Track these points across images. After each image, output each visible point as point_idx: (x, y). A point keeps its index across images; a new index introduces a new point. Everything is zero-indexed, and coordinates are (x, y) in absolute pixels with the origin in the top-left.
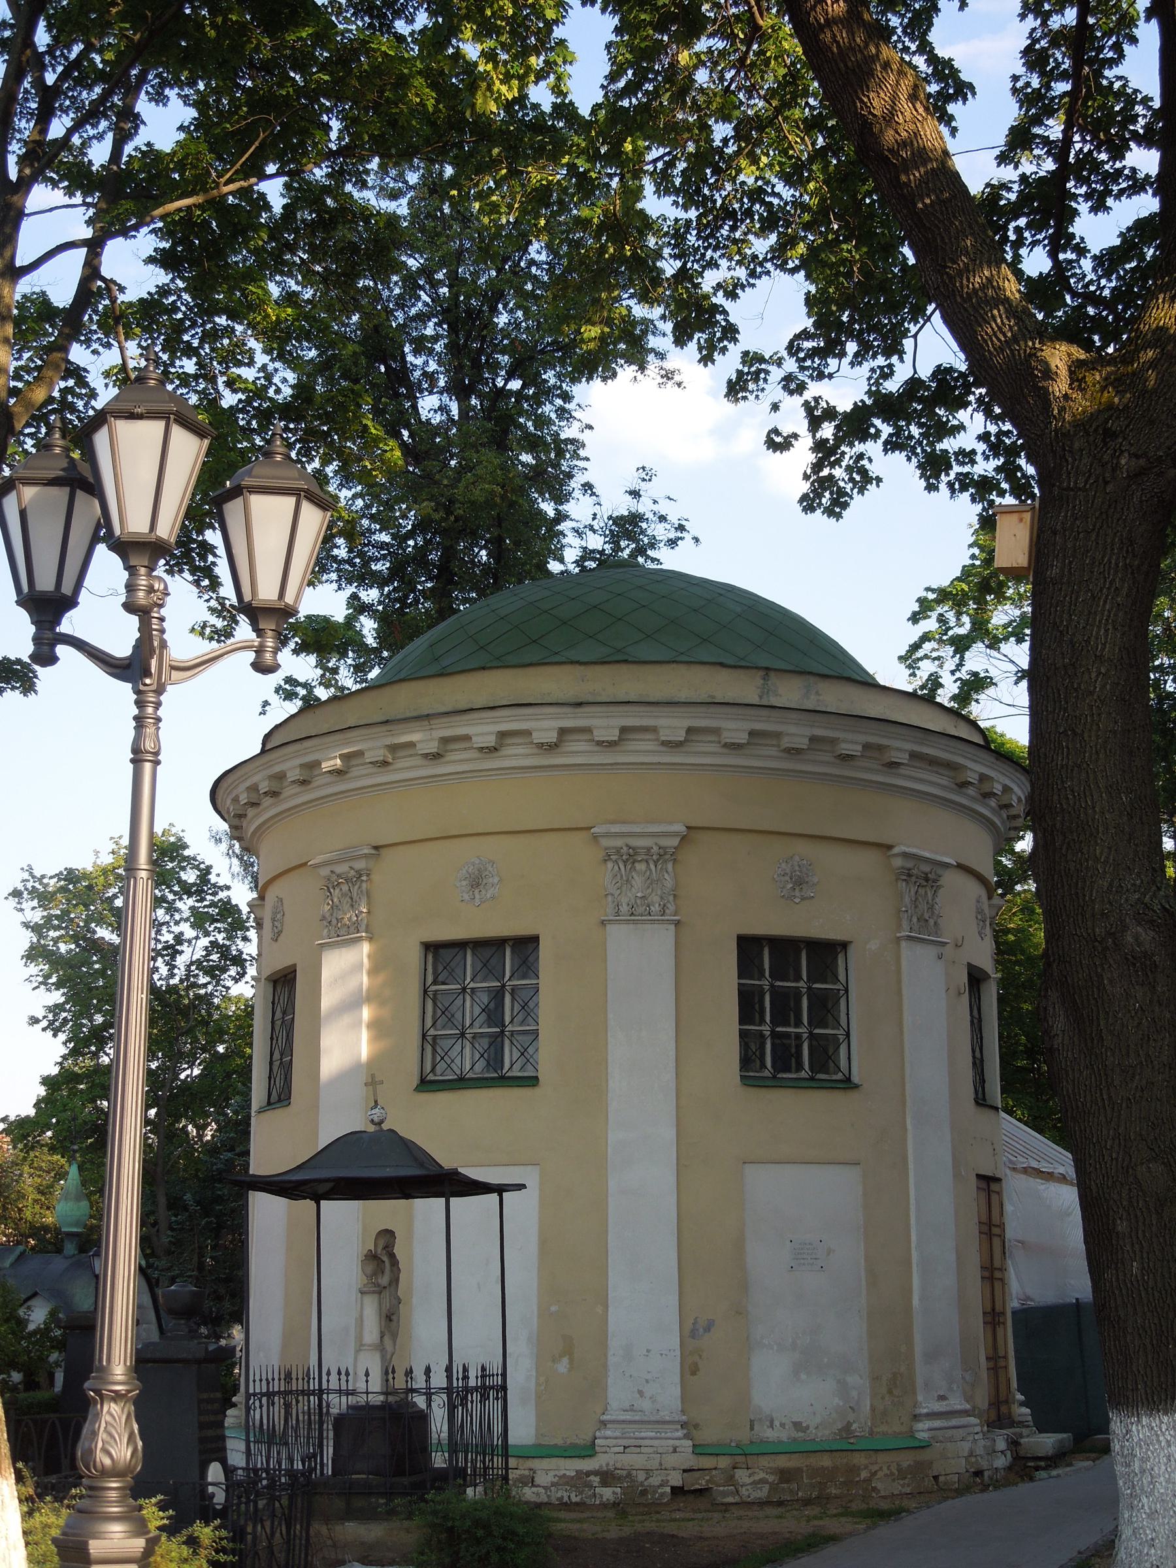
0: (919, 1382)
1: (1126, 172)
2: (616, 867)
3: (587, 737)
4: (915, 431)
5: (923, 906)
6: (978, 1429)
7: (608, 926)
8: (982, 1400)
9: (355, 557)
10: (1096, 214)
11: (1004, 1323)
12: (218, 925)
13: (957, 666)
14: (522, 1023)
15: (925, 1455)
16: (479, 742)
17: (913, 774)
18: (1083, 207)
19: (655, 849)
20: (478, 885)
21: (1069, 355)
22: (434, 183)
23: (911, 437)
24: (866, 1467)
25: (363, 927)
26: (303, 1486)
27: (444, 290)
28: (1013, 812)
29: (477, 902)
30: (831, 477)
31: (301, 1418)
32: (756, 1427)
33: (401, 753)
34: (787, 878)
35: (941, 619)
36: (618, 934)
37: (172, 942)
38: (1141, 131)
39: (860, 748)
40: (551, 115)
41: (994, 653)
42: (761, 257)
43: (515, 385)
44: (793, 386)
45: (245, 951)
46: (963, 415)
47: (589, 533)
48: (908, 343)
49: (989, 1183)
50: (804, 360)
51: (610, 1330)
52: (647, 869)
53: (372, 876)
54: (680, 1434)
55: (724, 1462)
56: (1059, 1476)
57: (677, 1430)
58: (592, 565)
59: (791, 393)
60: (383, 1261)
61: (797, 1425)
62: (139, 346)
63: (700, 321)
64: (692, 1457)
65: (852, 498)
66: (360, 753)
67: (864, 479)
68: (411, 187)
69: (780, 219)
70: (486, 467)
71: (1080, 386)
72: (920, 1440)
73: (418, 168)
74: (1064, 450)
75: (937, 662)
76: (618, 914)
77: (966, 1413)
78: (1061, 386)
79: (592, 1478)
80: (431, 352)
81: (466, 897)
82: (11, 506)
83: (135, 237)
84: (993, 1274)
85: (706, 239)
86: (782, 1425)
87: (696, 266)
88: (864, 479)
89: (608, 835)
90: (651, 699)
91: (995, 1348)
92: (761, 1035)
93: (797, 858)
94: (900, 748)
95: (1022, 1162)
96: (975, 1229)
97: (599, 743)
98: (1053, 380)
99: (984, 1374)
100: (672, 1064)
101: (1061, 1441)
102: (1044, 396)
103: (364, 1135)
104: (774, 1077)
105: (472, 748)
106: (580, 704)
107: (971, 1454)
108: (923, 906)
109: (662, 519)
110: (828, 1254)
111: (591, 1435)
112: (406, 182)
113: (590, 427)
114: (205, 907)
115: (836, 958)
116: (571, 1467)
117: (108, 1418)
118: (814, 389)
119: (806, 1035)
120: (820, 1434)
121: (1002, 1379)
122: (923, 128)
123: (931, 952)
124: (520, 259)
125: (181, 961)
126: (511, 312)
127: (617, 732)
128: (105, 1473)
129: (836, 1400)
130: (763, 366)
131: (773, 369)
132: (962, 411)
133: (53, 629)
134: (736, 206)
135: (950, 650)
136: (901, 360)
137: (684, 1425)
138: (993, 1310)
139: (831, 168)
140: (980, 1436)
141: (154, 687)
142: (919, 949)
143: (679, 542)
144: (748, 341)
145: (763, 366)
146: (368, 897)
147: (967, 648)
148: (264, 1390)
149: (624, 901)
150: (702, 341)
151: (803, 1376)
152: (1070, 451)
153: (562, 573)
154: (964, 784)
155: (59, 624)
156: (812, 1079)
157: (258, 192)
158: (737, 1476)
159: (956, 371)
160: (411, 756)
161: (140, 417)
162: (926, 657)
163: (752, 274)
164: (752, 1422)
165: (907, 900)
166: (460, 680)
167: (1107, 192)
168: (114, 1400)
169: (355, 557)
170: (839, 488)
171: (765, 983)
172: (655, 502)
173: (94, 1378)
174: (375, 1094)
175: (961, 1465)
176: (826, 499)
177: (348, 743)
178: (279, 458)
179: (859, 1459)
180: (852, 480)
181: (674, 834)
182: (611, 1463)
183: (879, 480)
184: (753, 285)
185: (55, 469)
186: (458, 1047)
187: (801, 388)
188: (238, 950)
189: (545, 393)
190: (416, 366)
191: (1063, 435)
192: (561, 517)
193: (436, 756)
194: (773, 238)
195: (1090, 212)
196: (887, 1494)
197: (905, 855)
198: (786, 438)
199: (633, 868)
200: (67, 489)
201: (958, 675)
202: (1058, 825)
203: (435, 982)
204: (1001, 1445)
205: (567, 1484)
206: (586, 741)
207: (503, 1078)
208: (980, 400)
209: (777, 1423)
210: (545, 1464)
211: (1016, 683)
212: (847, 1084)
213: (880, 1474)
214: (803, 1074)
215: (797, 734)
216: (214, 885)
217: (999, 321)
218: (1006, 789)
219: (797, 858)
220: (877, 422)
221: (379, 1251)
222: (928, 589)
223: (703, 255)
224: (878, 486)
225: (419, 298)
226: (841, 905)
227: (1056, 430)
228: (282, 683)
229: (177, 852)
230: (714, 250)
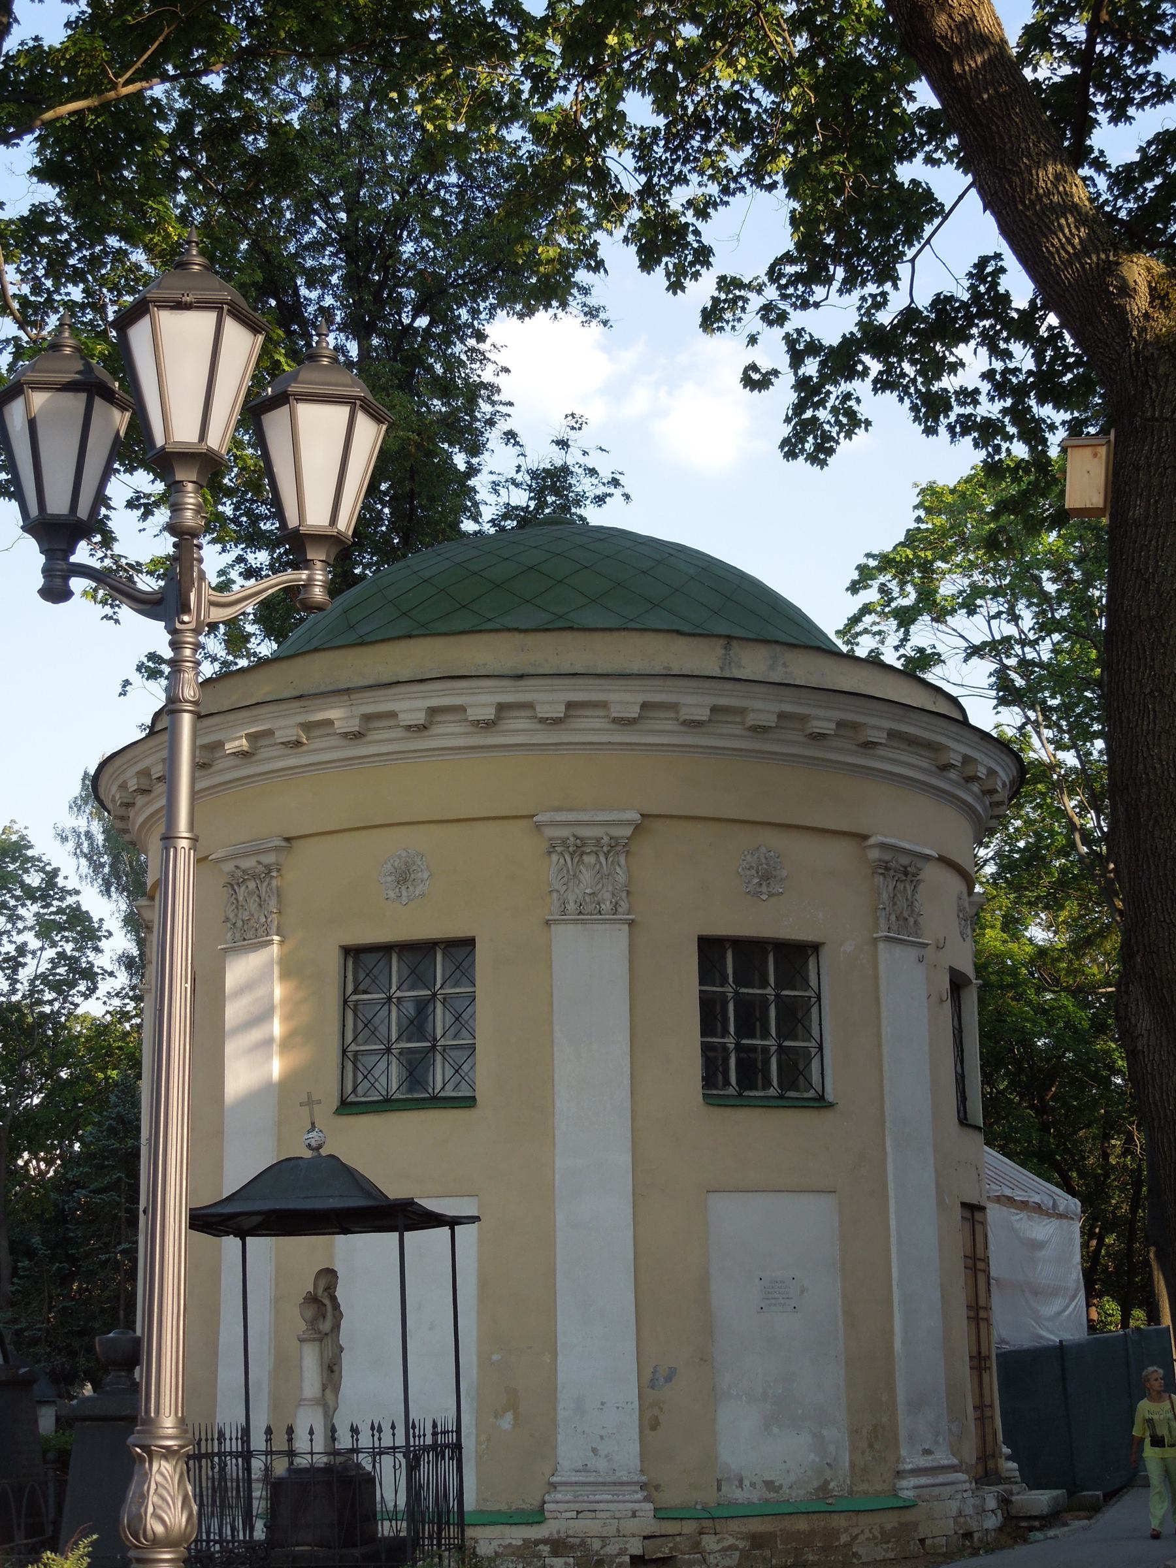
0: (902, 1432)
1: (1150, 78)
2: (562, 860)
3: (529, 713)
4: (908, 368)
5: (902, 903)
6: (967, 1486)
7: (553, 927)
8: (970, 1454)
9: (241, 515)
10: (1116, 125)
11: (990, 1368)
12: (66, 934)
13: (902, 641)
14: (455, 1037)
15: (910, 1516)
16: (407, 719)
17: (890, 755)
18: (1103, 116)
19: (606, 840)
20: (405, 880)
21: (1149, 269)
22: (330, 95)
23: (903, 375)
24: (846, 1530)
25: (274, 929)
26: (262, 1559)
27: (343, 216)
28: (997, 798)
29: (404, 900)
30: (814, 419)
31: (204, 1485)
32: (723, 1488)
33: (316, 732)
34: (753, 872)
35: (883, 589)
36: (563, 934)
37: (13, 953)
38: (1169, 33)
39: (833, 726)
40: (492, 11)
41: (942, 627)
42: (735, 171)
43: (423, 322)
44: (772, 316)
45: (96, 963)
46: (963, 351)
47: (511, 487)
48: (903, 269)
49: (973, 1211)
50: (786, 287)
51: (560, 1381)
52: (596, 861)
53: (283, 872)
54: (639, 1496)
55: (689, 1528)
56: (1056, 1537)
57: (636, 1492)
58: (510, 524)
59: (771, 323)
60: (322, 1302)
61: (769, 1485)
62: (18, 270)
63: (666, 244)
64: (653, 1521)
65: (838, 443)
66: (269, 733)
67: (852, 422)
68: (304, 99)
69: (755, 129)
70: (400, 412)
71: (1162, 303)
72: (905, 1500)
73: (312, 78)
74: (1147, 375)
75: (878, 638)
76: (564, 913)
77: (953, 1468)
78: (1140, 303)
79: (541, 1547)
80: (325, 285)
81: (392, 895)
82: (16, 415)
83: (17, 145)
84: (978, 1314)
85: (674, 151)
86: (753, 1485)
87: (663, 181)
88: (852, 422)
89: (553, 824)
90: (600, 671)
91: (981, 1396)
92: (724, 1048)
93: (763, 850)
94: (878, 726)
95: (996, 1190)
96: (960, 1264)
97: (543, 721)
98: (1130, 296)
99: (972, 1425)
100: (627, 1081)
101: (1056, 1498)
102: (1120, 315)
103: (300, 1162)
104: (740, 1095)
105: (398, 726)
106: (520, 677)
107: (960, 1513)
108: (902, 903)
109: (592, 472)
110: (802, 1292)
111: (538, 1498)
112: (298, 94)
113: (506, 370)
114: (52, 913)
115: (806, 962)
116: (517, 1535)
117: (159, 1478)
118: (797, 319)
119: (774, 1048)
120: (794, 1494)
121: (989, 1430)
122: (980, 13)
123: (912, 954)
124: (429, 181)
125: (24, 974)
126: (417, 241)
127: (563, 708)
128: (157, 1542)
129: (812, 1456)
130: (742, 293)
131: (752, 296)
132: (962, 346)
133: (66, 559)
134: (710, 113)
135: (893, 623)
136: (896, 287)
137: (643, 1486)
138: (980, 1353)
139: (820, 71)
140: (970, 1494)
141: (192, 626)
142: (898, 950)
143: (608, 499)
144: (722, 264)
145: (742, 293)
146: (278, 896)
147: (913, 621)
148: (216, 1450)
149: (571, 898)
150: (671, 267)
151: (775, 1430)
152: (1154, 377)
153: (476, 533)
154: (946, 767)
155: (73, 553)
156: (782, 1097)
157: (152, 98)
158: (703, 1543)
159: (957, 300)
160: (328, 735)
161: (188, 307)
162: (866, 631)
163: (725, 190)
164: (719, 1482)
165: (885, 896)
166: (383, 650)
167: (1129, 101)
168: (165, 1457)
169: (241, 515)
170: (824, 431)
171: (729, 990)
172: (585, 453)
173: (139, 1432)
174: (312, 1115)
175: (949, 1527)
176: (809, 446)
177: (255, 720)
178: (325, 361)
179: (839, 1522)
180: (838, 422)
181: (628, 823)
182: (563, 1530)
183: (868, 423)
184: (727, 203)
185: (70, 372)
186: (383, 1065)
187: (782, 318)
188: (88, 962)
189: (456, 330)
190: (310, 300)
191: (1146, 358)
192: (472, 471)
193: (357, 736)
194: (748, 151)
195: (1109, 123)
196: (869, 1559)
197: (883, 846)
198: (765, 375)
199: (581, 861)
200: (83, 396)
201: (902, 651)
202: (1144, 798)
203: (355, 992)
204: (991, 1504)
205: (513, 1554)
206: (528, 718)
207: (434, 1098)
208: (984, 334)
209: (747, 1482)
210: (496, 1531)
211: (965, 661)
212: (821, 1102)
213: (861, 1538)
214: (771, 1092)
215: (764, 709)
216: (62, 890)
217: (1067, 231)
218: (991, 772)
219: (763, 850)
220: (866, 358)
221: (320, 1292)
222: (868, 555)
223: (671, 169)
224: (867, 430)
225: (314, 224)
226: (812, 904)
227: (1137, 353)
228: (145, 660)
229: (20, 852)
230: (684, 164)
